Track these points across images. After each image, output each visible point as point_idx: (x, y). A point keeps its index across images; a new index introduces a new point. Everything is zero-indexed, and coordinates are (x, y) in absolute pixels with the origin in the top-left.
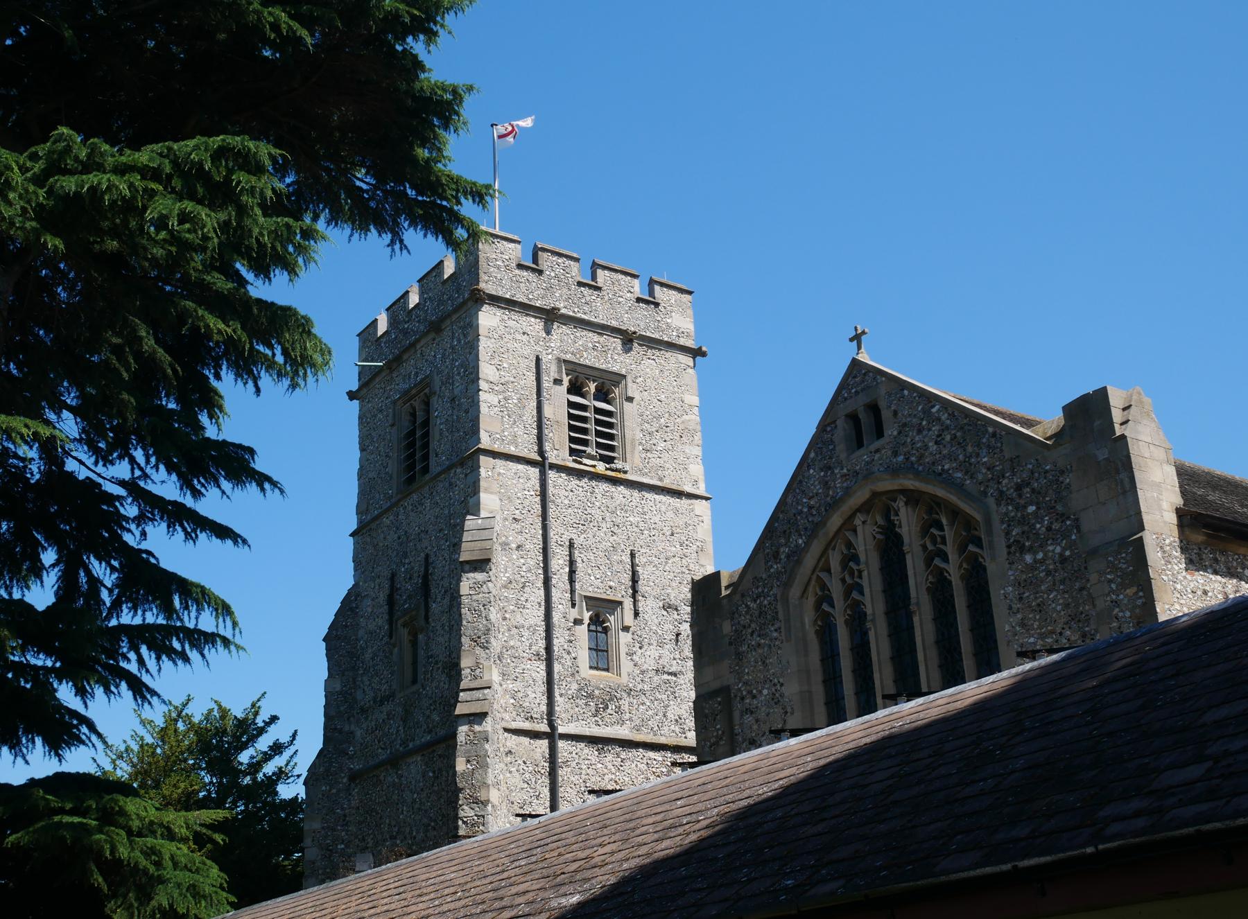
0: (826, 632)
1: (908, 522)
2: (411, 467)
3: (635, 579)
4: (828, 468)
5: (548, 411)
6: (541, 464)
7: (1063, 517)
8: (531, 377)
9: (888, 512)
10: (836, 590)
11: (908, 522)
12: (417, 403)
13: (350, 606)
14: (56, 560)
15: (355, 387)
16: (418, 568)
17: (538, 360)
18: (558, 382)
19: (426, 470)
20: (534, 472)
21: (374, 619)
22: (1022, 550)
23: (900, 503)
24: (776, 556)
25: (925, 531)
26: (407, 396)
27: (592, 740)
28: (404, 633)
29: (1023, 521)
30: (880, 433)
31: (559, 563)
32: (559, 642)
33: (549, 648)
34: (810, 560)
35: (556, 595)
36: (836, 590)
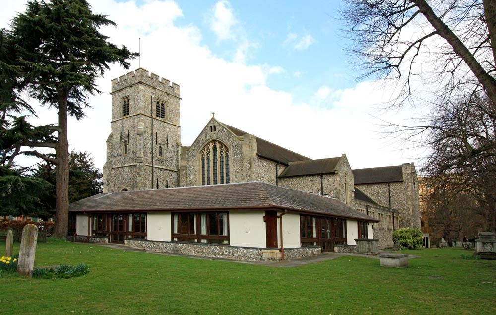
0: (203, 159)
1: (218, 146)
2: (125, 112)
3: (167, 140)
4: (206, 134)
5: (153, 108)
6: (152, 117)
7: (241, 152)
8: (150, 100)
9: (215, 143)
10: (205, 154)
11: (218, 146)
12: (126, 100)
13: (111, 137)
14: (266, 219)
15: (111, 92)
16: (127, 133)
17: (151, 97)
18: (155, 101)
19: (128, 114)
20: (150, 119)
21: (117, 139)
22: (235, 155)
23: (217, 143)
24: (196, 146)
25: (221, 148)
26: (124, 98)
27: (159, 168)
28: (124, 144)
29: (235, 151)
30: (215, 131)
31: (154, 136)
32: (154, 150)
33: (152, 152)
34: (202, 148)
35: (153, 142)
36: (205, 154)
